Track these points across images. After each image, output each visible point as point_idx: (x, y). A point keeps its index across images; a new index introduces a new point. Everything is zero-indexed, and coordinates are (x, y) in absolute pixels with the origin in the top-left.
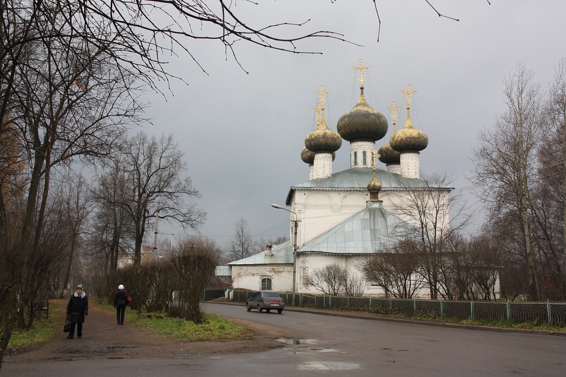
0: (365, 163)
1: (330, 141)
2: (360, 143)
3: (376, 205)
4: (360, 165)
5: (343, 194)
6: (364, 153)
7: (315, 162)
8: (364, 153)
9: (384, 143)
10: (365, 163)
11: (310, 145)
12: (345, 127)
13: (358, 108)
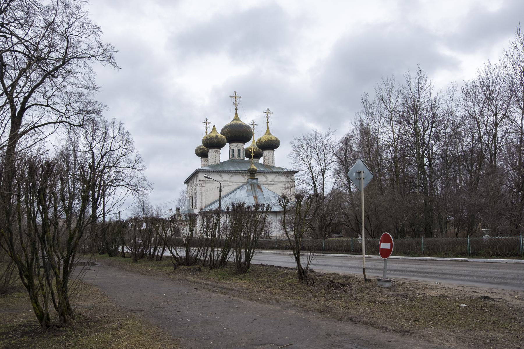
0: (239, 156)
1: (220, 141)
2: (236, 144)
3: (255, 181)
4: (236, 157)
5: (230, 175)
6: (239, 150)
7: (209, 155)
8: (239, 150)
9: (248, 145)
10: (239, 156)
11: (207, 143)
12: (227, 133)
13: (235, 122)
